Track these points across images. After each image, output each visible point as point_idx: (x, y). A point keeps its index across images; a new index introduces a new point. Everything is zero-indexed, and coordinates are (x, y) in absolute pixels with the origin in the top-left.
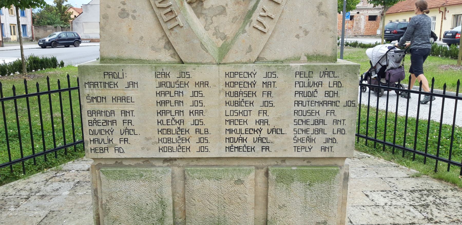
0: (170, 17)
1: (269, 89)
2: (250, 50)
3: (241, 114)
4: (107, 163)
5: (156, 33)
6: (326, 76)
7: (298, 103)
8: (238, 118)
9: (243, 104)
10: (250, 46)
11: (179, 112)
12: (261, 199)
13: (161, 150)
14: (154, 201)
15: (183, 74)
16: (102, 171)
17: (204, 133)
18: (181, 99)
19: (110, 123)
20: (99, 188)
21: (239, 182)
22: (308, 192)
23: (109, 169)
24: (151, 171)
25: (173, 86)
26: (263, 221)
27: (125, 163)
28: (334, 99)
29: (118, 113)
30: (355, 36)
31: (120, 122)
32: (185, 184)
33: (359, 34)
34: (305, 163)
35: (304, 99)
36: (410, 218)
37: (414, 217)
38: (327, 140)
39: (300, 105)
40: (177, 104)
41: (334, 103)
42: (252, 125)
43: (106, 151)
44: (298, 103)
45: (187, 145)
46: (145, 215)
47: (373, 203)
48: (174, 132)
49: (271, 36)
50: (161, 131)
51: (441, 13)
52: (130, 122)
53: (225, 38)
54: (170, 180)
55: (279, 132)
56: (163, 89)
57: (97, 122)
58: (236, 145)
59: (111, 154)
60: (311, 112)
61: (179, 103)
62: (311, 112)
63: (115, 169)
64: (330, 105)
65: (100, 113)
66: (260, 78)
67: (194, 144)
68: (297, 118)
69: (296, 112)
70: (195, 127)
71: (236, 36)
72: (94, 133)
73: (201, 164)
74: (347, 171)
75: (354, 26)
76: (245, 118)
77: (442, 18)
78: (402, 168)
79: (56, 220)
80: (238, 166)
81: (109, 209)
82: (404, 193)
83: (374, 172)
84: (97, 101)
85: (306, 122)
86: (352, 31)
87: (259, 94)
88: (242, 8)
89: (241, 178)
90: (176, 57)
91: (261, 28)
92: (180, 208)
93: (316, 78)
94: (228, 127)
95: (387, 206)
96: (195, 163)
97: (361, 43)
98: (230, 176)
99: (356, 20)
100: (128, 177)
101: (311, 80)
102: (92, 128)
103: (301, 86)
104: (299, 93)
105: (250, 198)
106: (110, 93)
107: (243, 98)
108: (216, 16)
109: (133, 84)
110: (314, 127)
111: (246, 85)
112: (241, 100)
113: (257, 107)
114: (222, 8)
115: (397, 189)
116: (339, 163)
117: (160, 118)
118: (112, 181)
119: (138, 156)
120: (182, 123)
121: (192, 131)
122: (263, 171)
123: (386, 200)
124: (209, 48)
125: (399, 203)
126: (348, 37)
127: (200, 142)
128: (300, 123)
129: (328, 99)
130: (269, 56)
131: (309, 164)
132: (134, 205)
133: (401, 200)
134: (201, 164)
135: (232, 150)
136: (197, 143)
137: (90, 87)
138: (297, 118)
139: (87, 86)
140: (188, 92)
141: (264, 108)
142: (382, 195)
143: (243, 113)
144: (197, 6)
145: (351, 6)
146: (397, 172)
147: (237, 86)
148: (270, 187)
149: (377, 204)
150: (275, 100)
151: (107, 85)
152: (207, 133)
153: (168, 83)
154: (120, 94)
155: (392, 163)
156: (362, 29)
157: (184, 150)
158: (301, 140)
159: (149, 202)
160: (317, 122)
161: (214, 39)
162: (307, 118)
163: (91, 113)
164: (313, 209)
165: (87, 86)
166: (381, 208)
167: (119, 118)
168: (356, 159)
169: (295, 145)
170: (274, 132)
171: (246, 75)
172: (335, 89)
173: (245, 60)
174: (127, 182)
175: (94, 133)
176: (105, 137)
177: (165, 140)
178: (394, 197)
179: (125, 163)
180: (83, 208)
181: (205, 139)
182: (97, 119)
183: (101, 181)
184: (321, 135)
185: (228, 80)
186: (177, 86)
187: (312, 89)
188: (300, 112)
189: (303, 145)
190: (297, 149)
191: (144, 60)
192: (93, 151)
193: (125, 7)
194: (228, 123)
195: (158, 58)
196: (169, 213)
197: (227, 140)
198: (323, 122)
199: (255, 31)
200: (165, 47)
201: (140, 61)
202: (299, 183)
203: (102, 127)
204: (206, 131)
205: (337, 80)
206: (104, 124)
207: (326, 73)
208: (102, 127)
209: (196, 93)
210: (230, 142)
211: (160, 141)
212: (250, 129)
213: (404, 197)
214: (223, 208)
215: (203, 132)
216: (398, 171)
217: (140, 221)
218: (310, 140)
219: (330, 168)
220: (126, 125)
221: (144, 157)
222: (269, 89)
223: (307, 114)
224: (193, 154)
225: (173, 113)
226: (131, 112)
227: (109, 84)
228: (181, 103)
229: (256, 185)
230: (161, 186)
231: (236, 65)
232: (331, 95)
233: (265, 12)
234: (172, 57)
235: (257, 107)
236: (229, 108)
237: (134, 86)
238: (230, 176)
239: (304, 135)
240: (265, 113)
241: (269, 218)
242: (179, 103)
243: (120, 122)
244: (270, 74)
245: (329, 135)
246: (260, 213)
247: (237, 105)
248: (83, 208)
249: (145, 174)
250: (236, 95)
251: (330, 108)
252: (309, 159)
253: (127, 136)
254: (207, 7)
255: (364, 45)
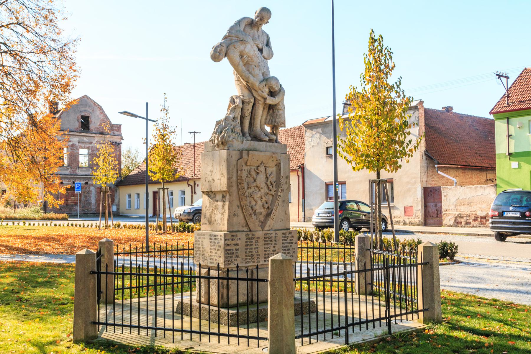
31: (235, 253)
44: (283, 243)
51: (190, 186)
57: (228, 253)
69: (283, 246)
77: (192, 193)
87: (273, 241)
143: (268, 248)
150: (277, 242)
185: (265, 236)
187: (286, 239)
204: (259, 255)
240: (275, 247)
243: (235, 253)
245: (291, 254)
251: (291, 244)
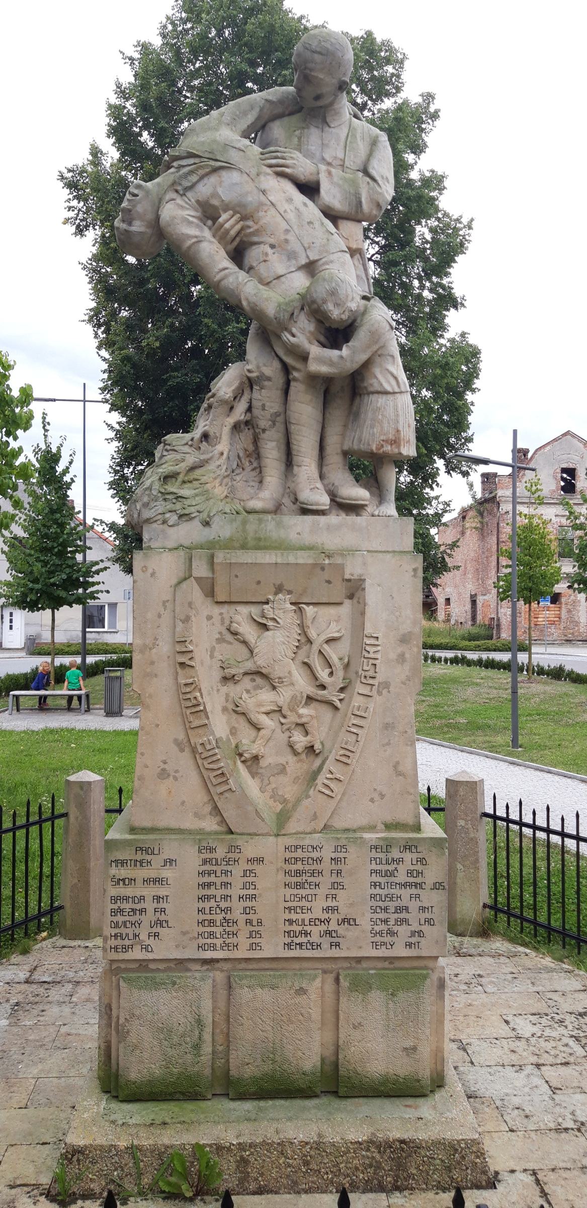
0: (220, 780)
1: (339, 867)
2: (315, 817)
3: (304, 899)
4: (128, 967)
5: (201, 797)
6: (408, 850)
7: (375, 885)
8: (301, 904)
9: (306, 886)
10: (315, 813)
11: (226, 897)
12: (330, 1016)
13: (200, 949)
14: (189, 1019)
15: (233, 848)
16: (122, 977)
18: (228, 880)
19: (138, 912)
20: (114, 1001)
21: (302, 991)
22: (391, 1005)
23: (131, 975)
24: (187, 977)
25: (219, 863)
26: (333, 1048)
27: (152, 966)
28: (419, 880)
29: (149, 899)
30: (567, 640)
31: (150, 911)
32: (230, 995)
33: (577, 636)
34: (386, 965)
35: (382, 880)
36: (564, 1055)
37: (571, 1054)
38: (413, 934)
39: (378, 887)
40: (223, 887)
42: (318, 913)
43: (130, 950)
44: (375, 885)
45: (234, 940)
46: (176, 1039)
47: (512, 1034)
48: (218, 924)
49: (341, 799)
50: (201, 923)
52: (163, 911)
53: (285, 801)
54: (211, 990)
55: (352, 923)
56: (207, 867)
57: (121, 911)
58: (297, 940)
59: (137, 954)
60: (390, 896)
61: (226, 885)
62: (390, 896)
63: (139, 975)
64: (413, 887)
65: (127, 899)
66: (327, 853)
67: (243, 940)
68: (374, 903)
69: (374, 897)
70: (245, 917)
71: (298, 801)
72: (117, 925)
73: (251, 967)
74: (442, 975)
75: (563, 617)
76: (308, 905)
78: (579, 975)
79: (5, 1066)
80: (300, 969)
81: (128, 1032)
82: (568, 1017)
83: (529, 982)
84: (124, 884)
85: (386, 909)
86: (560, 629)
88: (305, 766)
89: (303, 986)
90: (224, 825)
91: (327, 792)
92: (222, 1031)
93: (395, 854)
94: (287, 916)
95: (534, 1039)
96: (243, 965)
97: (572, 672)
98: (290, 983)
99: (566, 604)
100: (156, 985)
101: (390, 856)
102: (115, 919)
103: (378, 863)
104: (376, 872)
105: (316, 1014)
106: (141, 873)
107: (307, 878)
108: (274, 776)
109: (171, 861)
110: (396, 916)
111: (310, 861)
112: (304, 881)
113: (323, 891)
114: (282, 767)
115: (558, 1011)
116: (430, 964)
117: (201, 905)
118: (136, 992)
119: (171, 957)
120: (229, 912)
121: (241, 923)
122: (333, 975)
123: (535, 1029)
124: (265, 815)
125: (554, 1034)
126: (549, 644)
127: (251, 936)
128: (379, 910)
129: (411, 880)
130: (339, 823)
131: (392, 966)
132: (161, 1025)
133: (559, 1029)
134: (251, 967)
135: (292, 947)
137: (117, 866)
138: (374, 903)
139: (113, 864)
140: (237, 871)
141: (333, 892)
142: (530, 1021)
144: (252, 765)
145: (541, 587)
146: (568, 981)
147: (299, 863)
148: (341, 998)
149: (520, 1036)
150: (345, 880)
151: (138, 864)
152: (260, 924)
153: (214, 860)
154: (153, 874)
155: (564, 966)
156: (582, 625)
157: (230, 948)
158: (380, 933)
159: (183, 1020)
160: (398, 910)
161: (271, 802)
162: (386, 904)
163: (115, 899)
164: (399, 1028)
165: (113, 864)
166: (523, 1042)
167: (150, 906)
168: (502, 959)
169: (373, 940)
170: (346, 923)
171: (310, 849)
172: (419, 867)
173: (308, 830)
174: (154, 993)
175: (117, 925)
176: (130, 931)
177: (206, 934)
178: (550, 1023)
179: (152, 966)
180: (41, 1046)
181: (257, 932)
182: (121, 908)
183: (120, 992)
184: (404, 927)
185: (288, 855)
186: (225, 863)
188: (378, 896)
189: (382, 939)
190: (375, 945)
191: (184, 830)
192: (113, 950)
193: (166, 766)
194: (287, 911)
195: (201, 827)
196: (207, 1037)
197: (286, 934)
198: (407, 909)
199: (320, 795)
200: (210, 814)
201: (180, 831)
202: (379, 991)
203: (127, 918)
204: (260, 923)
205: (420, 856)
206: (130, 914)
207: (408, 846)
208: (127, 918)
209: (248, 872)
210: (289, 936)
211: (200, 937)
213: (567, 1023)
214: (279, 1029)
215: (255, 923)
216: (569, 979)
217: (168, 1049)
218: (392, 933)
219: (417, 972)
220: (158, 914)
221: (178, 957)
222: (339, 867)
223: (387, 899)
224: (242, 953)
225: (218, 899)
226: (165, 898)
227: (141, 862)
228: (229, 885)
229: (323, 996)
230: (199, 998)
231: (298, 836)
232: (415, 875)
233: (332, 774)
234: (219, 825)
235: (323, 891)
236: (289, 892)
237: (171, 865)
238: (290, 983)
239: (383, 927)
240: (334, 897)
241: (341, 1042)
242: (226, 885)
243: (150, 911)
244: (339, 847)
245: (415, 927)
246: (329, 1036)
247: (298, 887)
248: (41, 1046)
249: (178, 981)
250: (298, 875)
251: (414, 891)
252: (391, 960)
253: (158, 929)
254: (264, 766)
255: (578, 675)
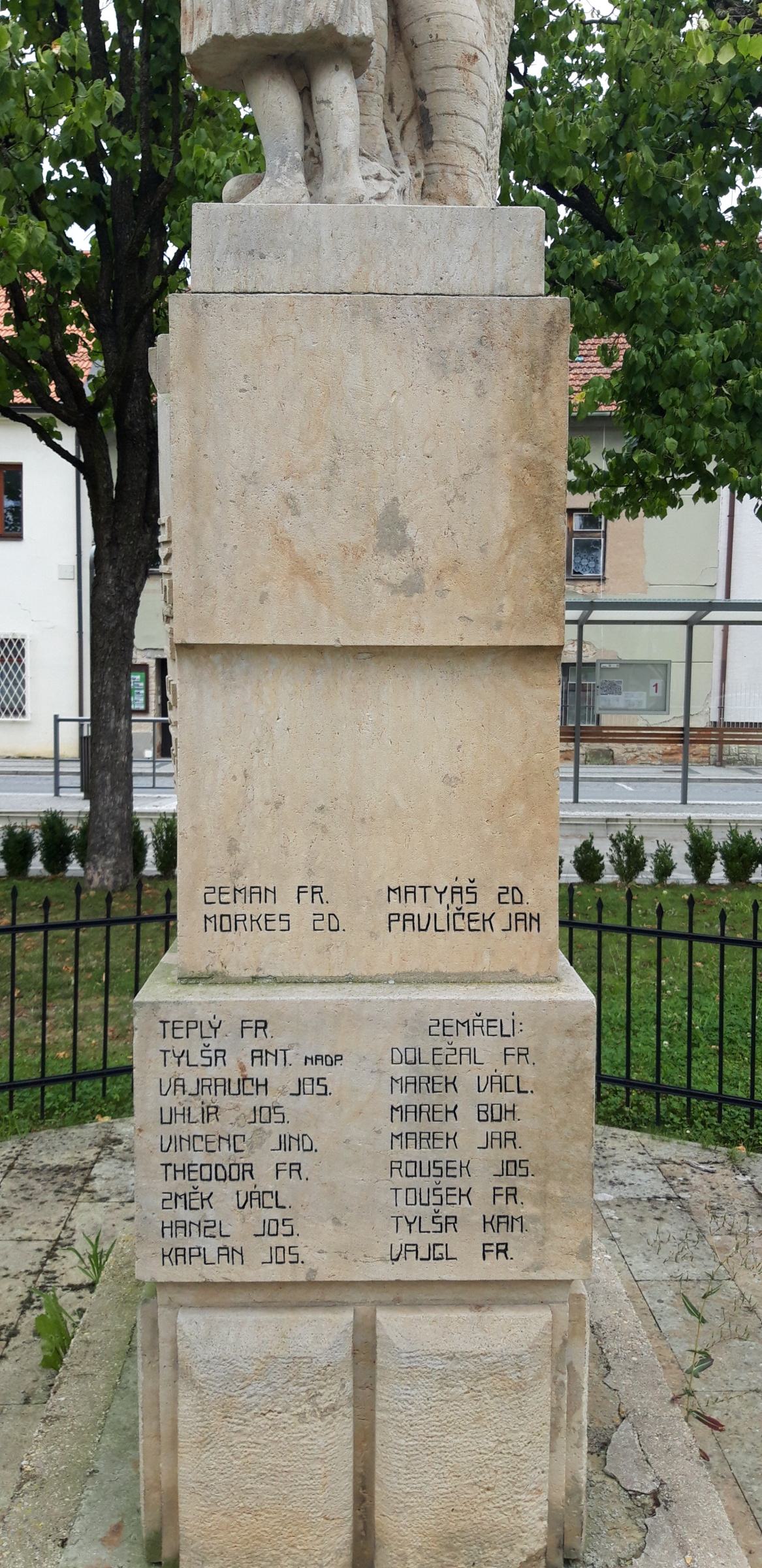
17: (417, 889)
41: (185, 1143)
136: (256, 1235)
212: (202, 1165)
